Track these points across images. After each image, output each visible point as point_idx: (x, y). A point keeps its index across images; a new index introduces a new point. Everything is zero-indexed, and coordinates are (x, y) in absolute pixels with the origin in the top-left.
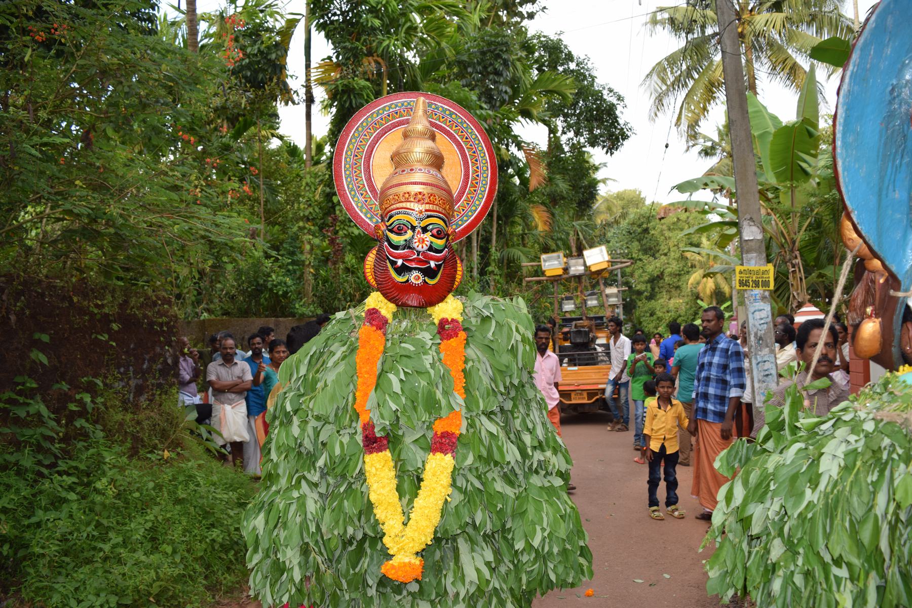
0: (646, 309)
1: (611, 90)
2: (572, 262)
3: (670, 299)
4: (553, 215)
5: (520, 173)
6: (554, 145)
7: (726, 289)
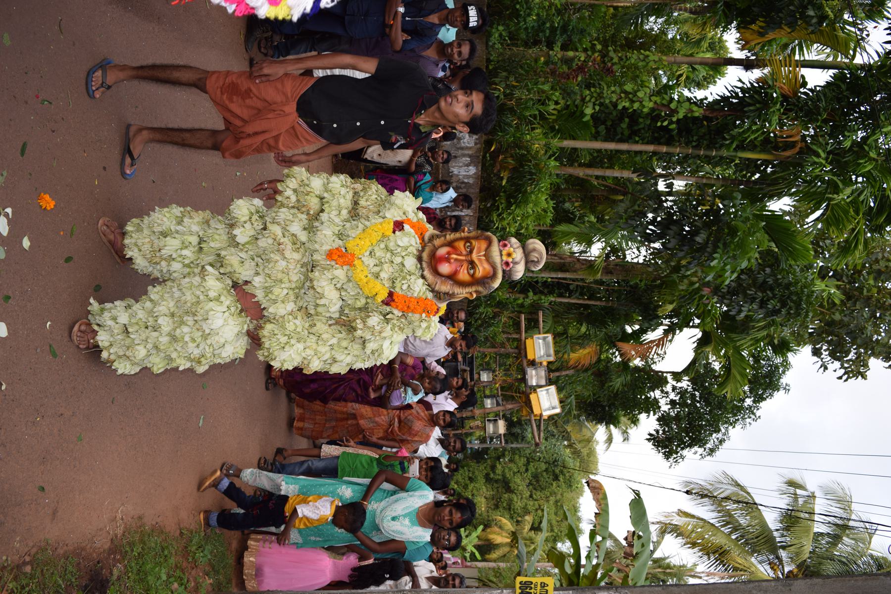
0: (477, 473)
1: (721, 442)
2: (543, 373)
3: (485, 498)
4: (586, 370)
5: (636, 335)
6: (659, 380)
7: (494, 556)
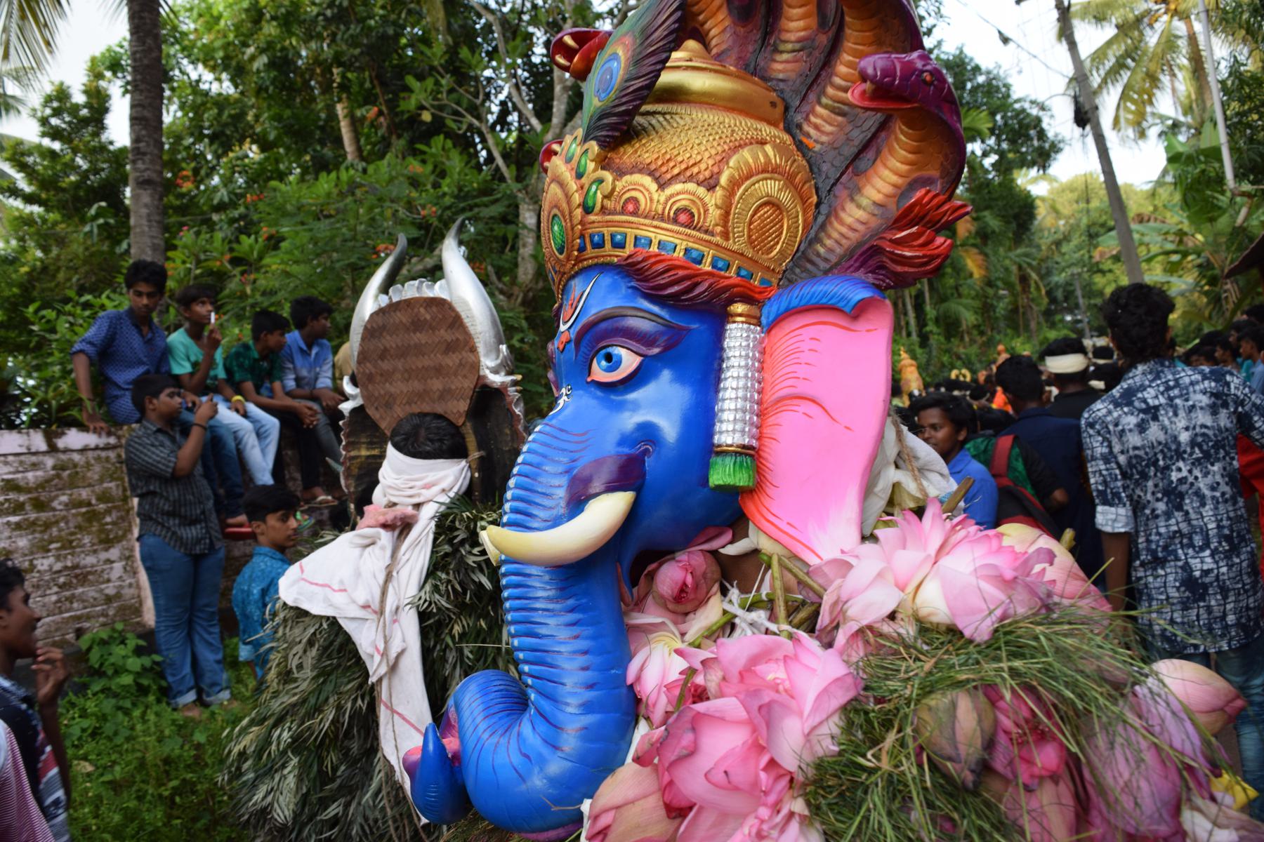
4: (986, 255)
